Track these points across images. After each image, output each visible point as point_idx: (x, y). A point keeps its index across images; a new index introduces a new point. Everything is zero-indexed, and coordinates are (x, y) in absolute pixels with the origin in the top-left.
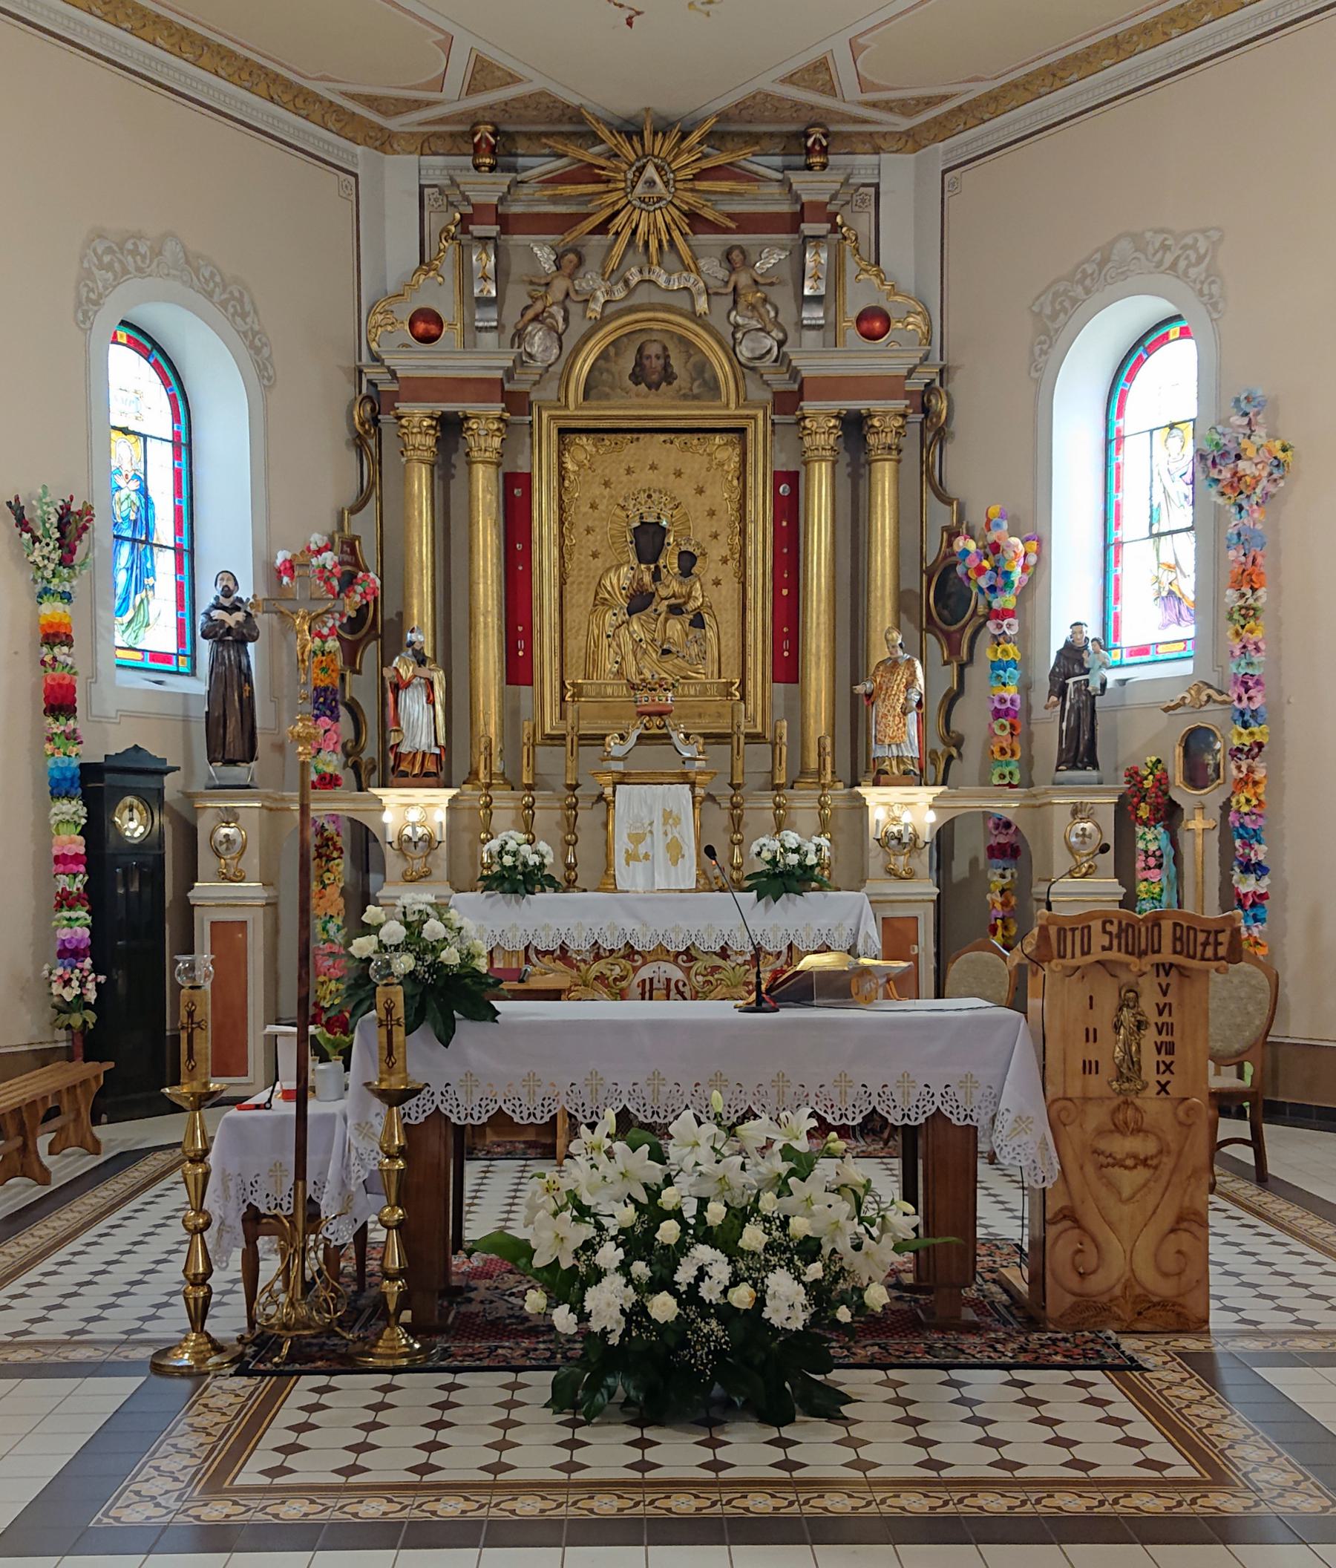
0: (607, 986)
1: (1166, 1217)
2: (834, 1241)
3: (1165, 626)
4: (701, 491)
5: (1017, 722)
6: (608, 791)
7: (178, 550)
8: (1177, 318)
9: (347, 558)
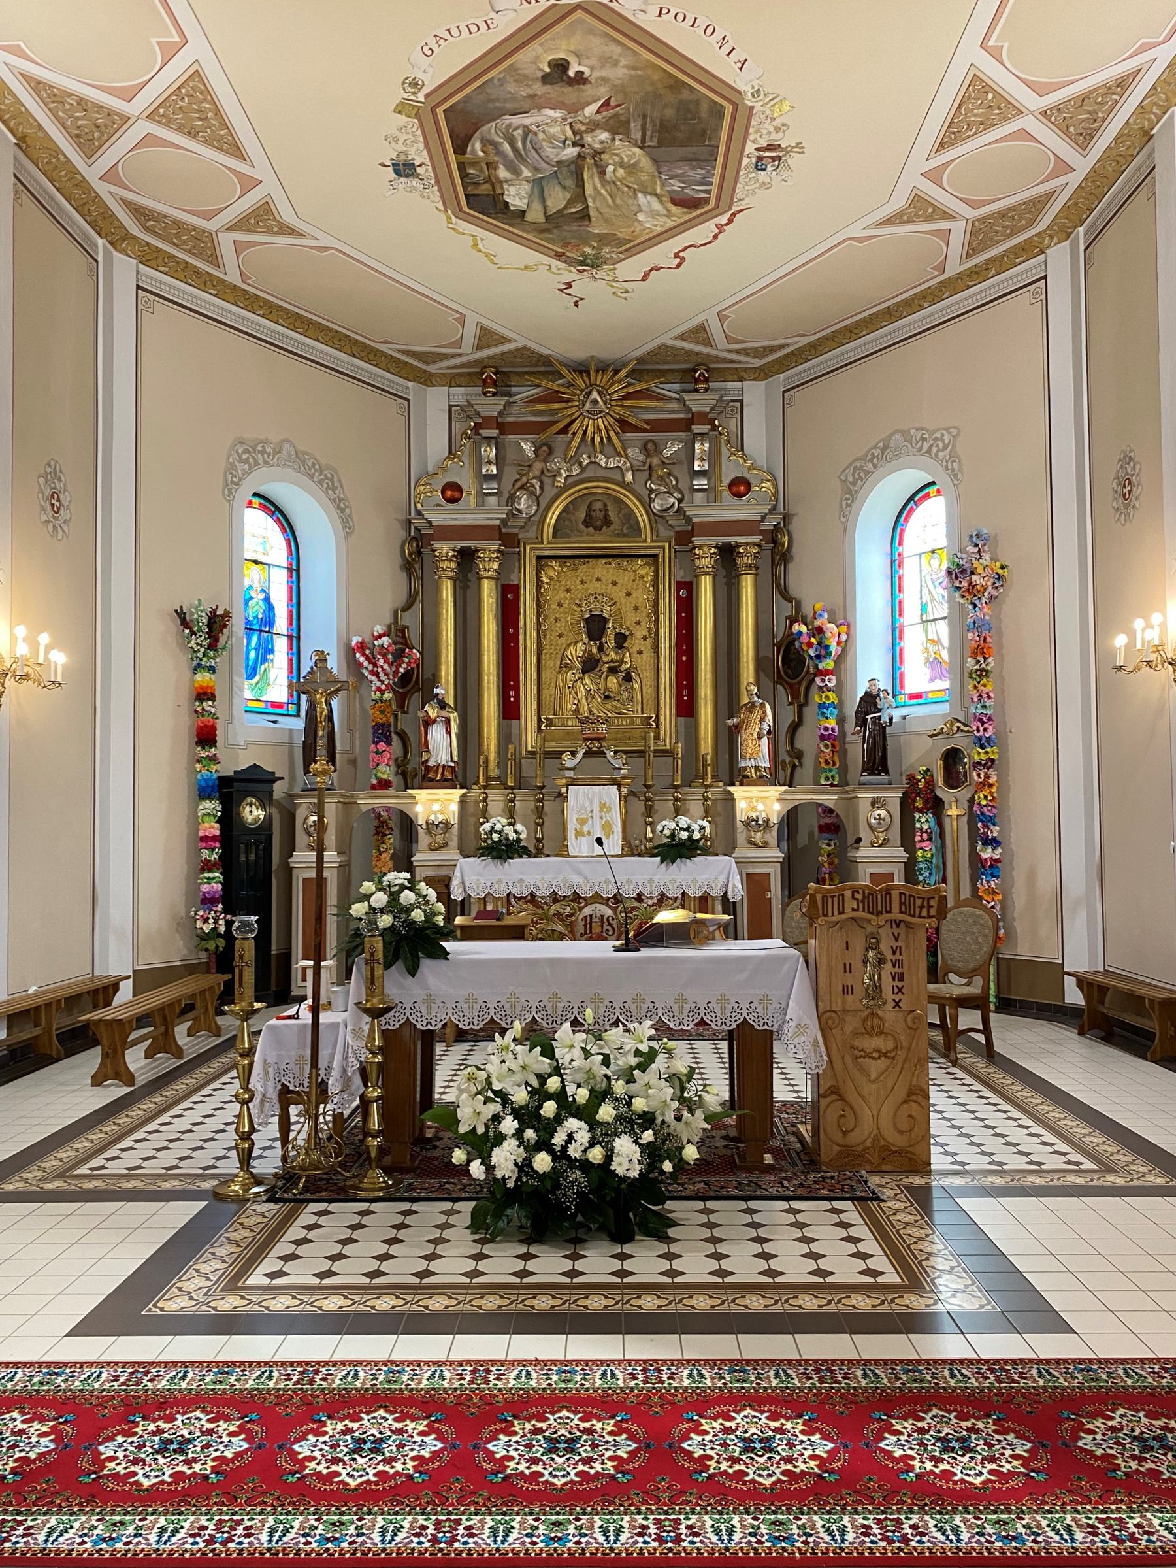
0: (562, 920)
1: (901, 1092)
2: (663, 1114)
3: (932, 680)
4: (634, 595)
5: (837, 744)
6: (564, 790)
7: (290, 637)
8: (933, 483)
9: (399, 640)
